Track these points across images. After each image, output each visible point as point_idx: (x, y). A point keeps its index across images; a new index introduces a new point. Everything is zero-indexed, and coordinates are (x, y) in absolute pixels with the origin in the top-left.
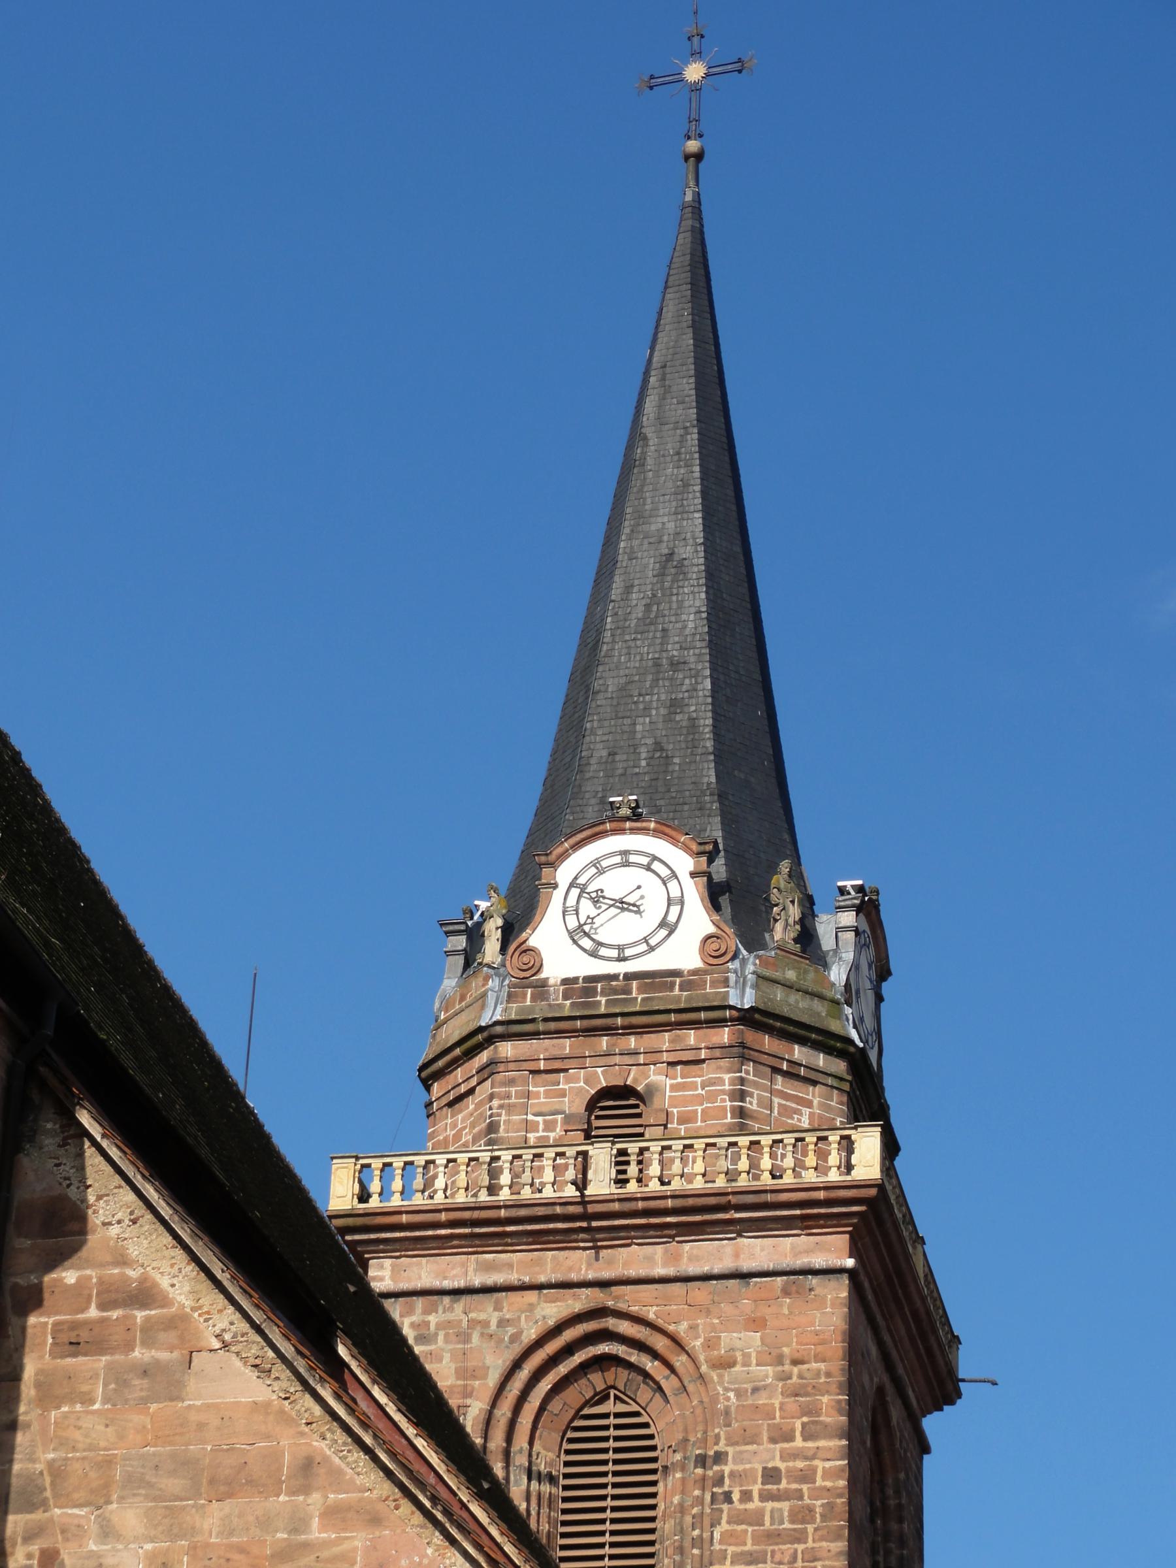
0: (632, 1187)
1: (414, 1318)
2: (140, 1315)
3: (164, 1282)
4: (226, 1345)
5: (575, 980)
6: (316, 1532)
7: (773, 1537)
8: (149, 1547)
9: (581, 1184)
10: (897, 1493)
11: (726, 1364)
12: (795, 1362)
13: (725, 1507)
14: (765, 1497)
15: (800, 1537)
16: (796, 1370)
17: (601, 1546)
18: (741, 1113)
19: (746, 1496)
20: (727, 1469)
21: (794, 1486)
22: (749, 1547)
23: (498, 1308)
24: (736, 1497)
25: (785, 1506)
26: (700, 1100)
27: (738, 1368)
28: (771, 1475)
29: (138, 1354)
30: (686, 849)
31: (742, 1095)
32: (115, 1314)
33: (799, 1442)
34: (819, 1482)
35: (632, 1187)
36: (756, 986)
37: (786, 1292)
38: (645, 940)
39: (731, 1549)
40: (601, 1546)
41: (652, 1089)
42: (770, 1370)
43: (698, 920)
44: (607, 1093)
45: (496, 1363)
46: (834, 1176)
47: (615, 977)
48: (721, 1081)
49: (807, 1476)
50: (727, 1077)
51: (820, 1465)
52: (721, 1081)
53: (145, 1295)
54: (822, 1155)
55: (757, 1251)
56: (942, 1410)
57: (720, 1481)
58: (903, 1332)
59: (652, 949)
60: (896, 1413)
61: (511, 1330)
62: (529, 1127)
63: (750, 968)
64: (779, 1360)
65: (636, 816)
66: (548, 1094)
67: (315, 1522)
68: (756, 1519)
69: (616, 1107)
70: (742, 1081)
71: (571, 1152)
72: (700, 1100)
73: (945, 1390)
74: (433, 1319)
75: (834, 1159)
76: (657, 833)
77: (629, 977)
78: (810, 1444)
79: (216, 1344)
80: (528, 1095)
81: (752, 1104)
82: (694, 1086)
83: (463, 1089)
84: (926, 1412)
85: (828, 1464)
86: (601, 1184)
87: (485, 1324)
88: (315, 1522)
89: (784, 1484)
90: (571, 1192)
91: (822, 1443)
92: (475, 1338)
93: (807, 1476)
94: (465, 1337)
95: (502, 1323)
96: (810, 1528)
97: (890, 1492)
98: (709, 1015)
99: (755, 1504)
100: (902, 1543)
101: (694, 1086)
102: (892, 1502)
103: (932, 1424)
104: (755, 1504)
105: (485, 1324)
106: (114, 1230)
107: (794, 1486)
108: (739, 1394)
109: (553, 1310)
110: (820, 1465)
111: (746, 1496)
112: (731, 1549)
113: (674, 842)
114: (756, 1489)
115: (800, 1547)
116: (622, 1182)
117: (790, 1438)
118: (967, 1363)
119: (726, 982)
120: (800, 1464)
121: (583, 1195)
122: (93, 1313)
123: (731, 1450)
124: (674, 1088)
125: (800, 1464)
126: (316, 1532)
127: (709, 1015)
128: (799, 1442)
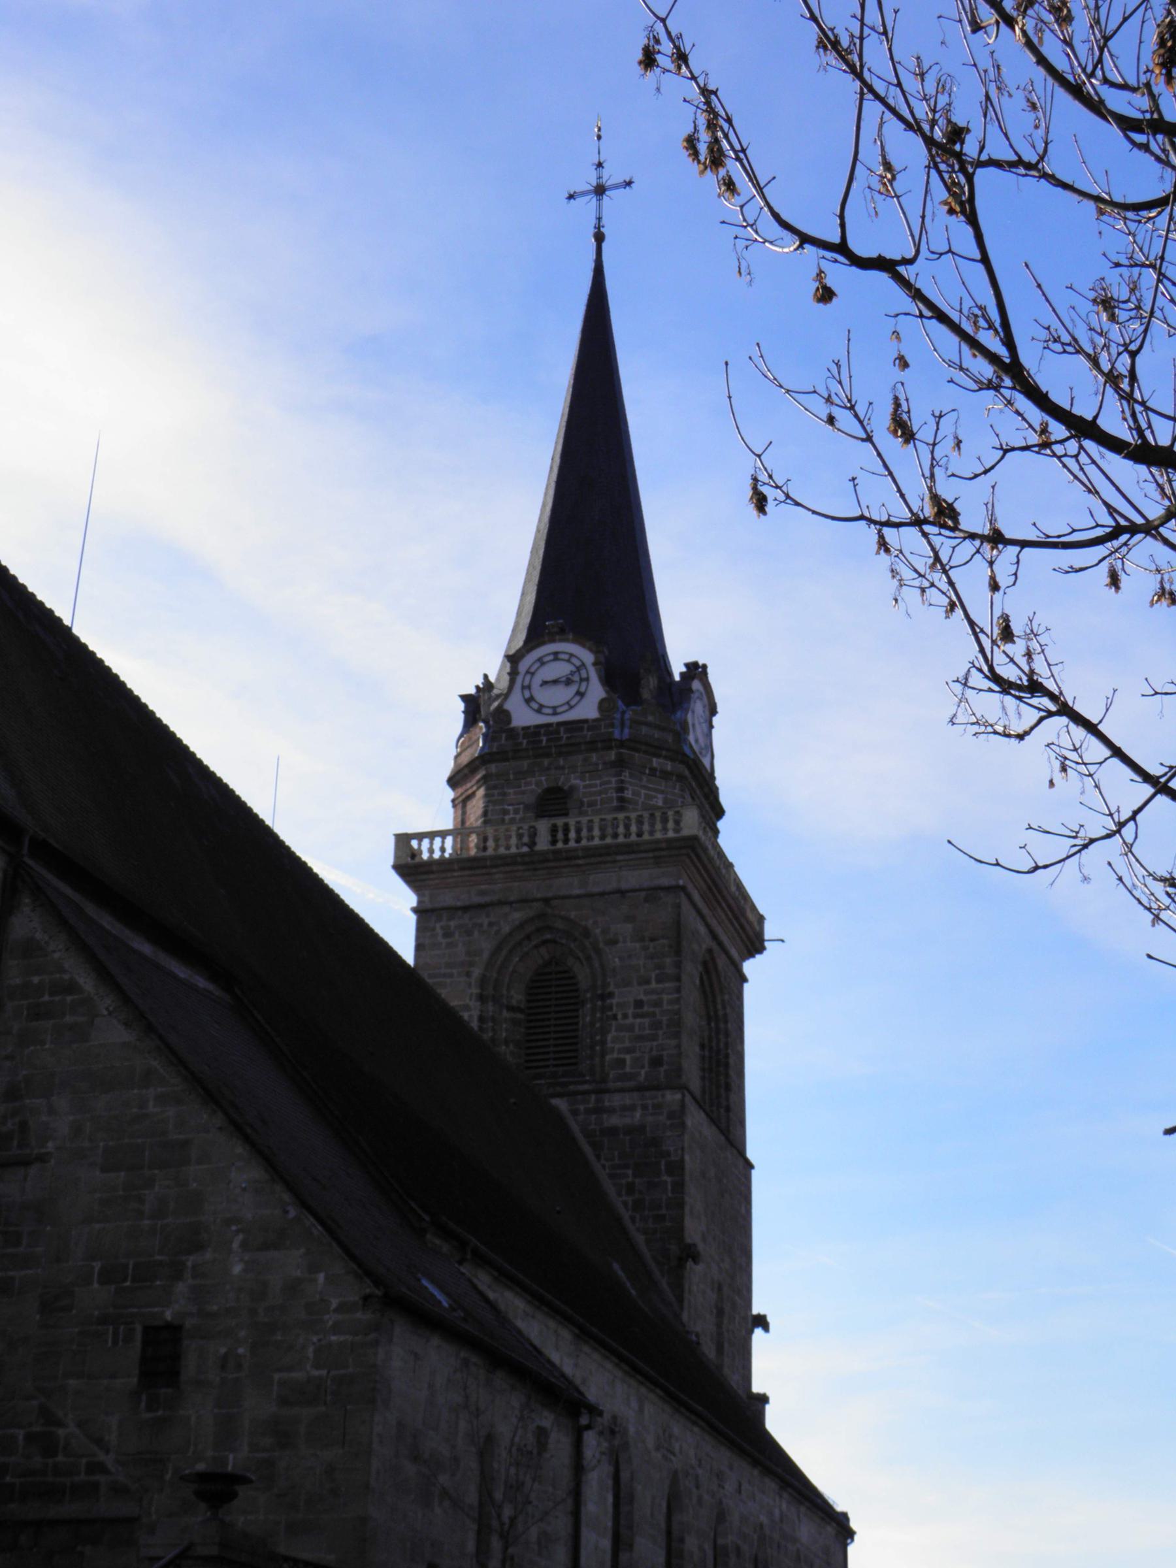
0: (560, 845)
1: (442, 923)
2: (69, 998)
3: (81, 981)
4: (110, 1013)
5: (528, 728)
6: (152, 1108)
7: (640, 1038)
8: (71, 1118)
9: (532, 844)
10: (724, 1008)
11: (614, 942)
12: (652, 940)
13: (614, 1023)
14: (636, 1016)
15: (654, 1038)
16: (652, 945)
17: (548, 1046)
18: (622, 800)
19: (625, 1016)
20: (614, 1001)
21: (652, 1009)
22: (627, 1044)
23: (488, 916)
24: (619, 1016)
25: (646, 1021)
26: (600, 793)
27: (620, 945)
28: (639, 1004)
29: (69, 1019)
30: (591, 650)
31: (621, 790)
32: (57, 998)
33: (654, 985)
34: (665, 1007)
35: (560, 845)
36: (631, 727)
37: (646, 900)
38: (568, 703)
39: (617, 1046)
40: (548, 1046)
41: (573, 789)
42: (638, 945)
43: (596, 691)
44: (548, 791)
45: (486, 946)
46: (671, 834)
47: (550, 725)
48: (609, 782)
49: (658, 1004)
50: (613, 780)
51: (665, 997)
52: (609, 782)
53: (71, 987)
54: (652, 825)
55: (634, 878)
56: (763, 1399)
57: (611, 1008)
58: (724, 917)
59: (571, 707)
60: (722, 961)
61: (495, 928)
62: (506, 812)
63: (627, 716)
64: (642, 939)
65: (562, 631)
66: (515, 793)
67: (151, 1103)
68: (630, 1028)
69: (553, 802)
70: (622, 781)
71: (526, 827)
72: (600, 793)
73: (755, 945)
74: (452, 924)
75: (671, 825)
76: (575, 641)
77: (559, 724)
78: (661, 986)
79: (105, 1013)
80: (504, 794)
81: (628, 794)
82: (596, 786)
83: (470, 792)
84: (745, 959)
85: (670, 997)
86: (543, 844)
87: (481, 925)
88: (151, 1103)
89: (646, 1009)
90: (525, 849)
91: (667, 985)
92: (476, 933)
93: (658, 1004)
94: (469, 933)
95: (491, 924)
96: (660, 1033)
97: (719, 1007)
98: (608, 743)
99: (630, 1020)
100: (727, 1035)
101: (596, 786)
102: (721, 1013)
103: (750, 967)
104: (630, 1020)
105: (481, 925)
106: (57, 955)
107: (652, 1009)
108: (621, 959)
109: (517, 916)
110: (665, 997)
111: (625, 1016)
112: (617, 1046)
113: (584, 646)
114: (630, 1011)
115: (655, 1043)
116: (554, 842)
117: (648, 982)
118: (769, 931)
119: (612, 725)
120: (654, 997)
121: (532, 850)
122: (46, 998)
123: (616, 991)
124: (585, 787)
125: (654, 997)
126: (152, 1108)
127: (608, 743)
128: (654, 985)
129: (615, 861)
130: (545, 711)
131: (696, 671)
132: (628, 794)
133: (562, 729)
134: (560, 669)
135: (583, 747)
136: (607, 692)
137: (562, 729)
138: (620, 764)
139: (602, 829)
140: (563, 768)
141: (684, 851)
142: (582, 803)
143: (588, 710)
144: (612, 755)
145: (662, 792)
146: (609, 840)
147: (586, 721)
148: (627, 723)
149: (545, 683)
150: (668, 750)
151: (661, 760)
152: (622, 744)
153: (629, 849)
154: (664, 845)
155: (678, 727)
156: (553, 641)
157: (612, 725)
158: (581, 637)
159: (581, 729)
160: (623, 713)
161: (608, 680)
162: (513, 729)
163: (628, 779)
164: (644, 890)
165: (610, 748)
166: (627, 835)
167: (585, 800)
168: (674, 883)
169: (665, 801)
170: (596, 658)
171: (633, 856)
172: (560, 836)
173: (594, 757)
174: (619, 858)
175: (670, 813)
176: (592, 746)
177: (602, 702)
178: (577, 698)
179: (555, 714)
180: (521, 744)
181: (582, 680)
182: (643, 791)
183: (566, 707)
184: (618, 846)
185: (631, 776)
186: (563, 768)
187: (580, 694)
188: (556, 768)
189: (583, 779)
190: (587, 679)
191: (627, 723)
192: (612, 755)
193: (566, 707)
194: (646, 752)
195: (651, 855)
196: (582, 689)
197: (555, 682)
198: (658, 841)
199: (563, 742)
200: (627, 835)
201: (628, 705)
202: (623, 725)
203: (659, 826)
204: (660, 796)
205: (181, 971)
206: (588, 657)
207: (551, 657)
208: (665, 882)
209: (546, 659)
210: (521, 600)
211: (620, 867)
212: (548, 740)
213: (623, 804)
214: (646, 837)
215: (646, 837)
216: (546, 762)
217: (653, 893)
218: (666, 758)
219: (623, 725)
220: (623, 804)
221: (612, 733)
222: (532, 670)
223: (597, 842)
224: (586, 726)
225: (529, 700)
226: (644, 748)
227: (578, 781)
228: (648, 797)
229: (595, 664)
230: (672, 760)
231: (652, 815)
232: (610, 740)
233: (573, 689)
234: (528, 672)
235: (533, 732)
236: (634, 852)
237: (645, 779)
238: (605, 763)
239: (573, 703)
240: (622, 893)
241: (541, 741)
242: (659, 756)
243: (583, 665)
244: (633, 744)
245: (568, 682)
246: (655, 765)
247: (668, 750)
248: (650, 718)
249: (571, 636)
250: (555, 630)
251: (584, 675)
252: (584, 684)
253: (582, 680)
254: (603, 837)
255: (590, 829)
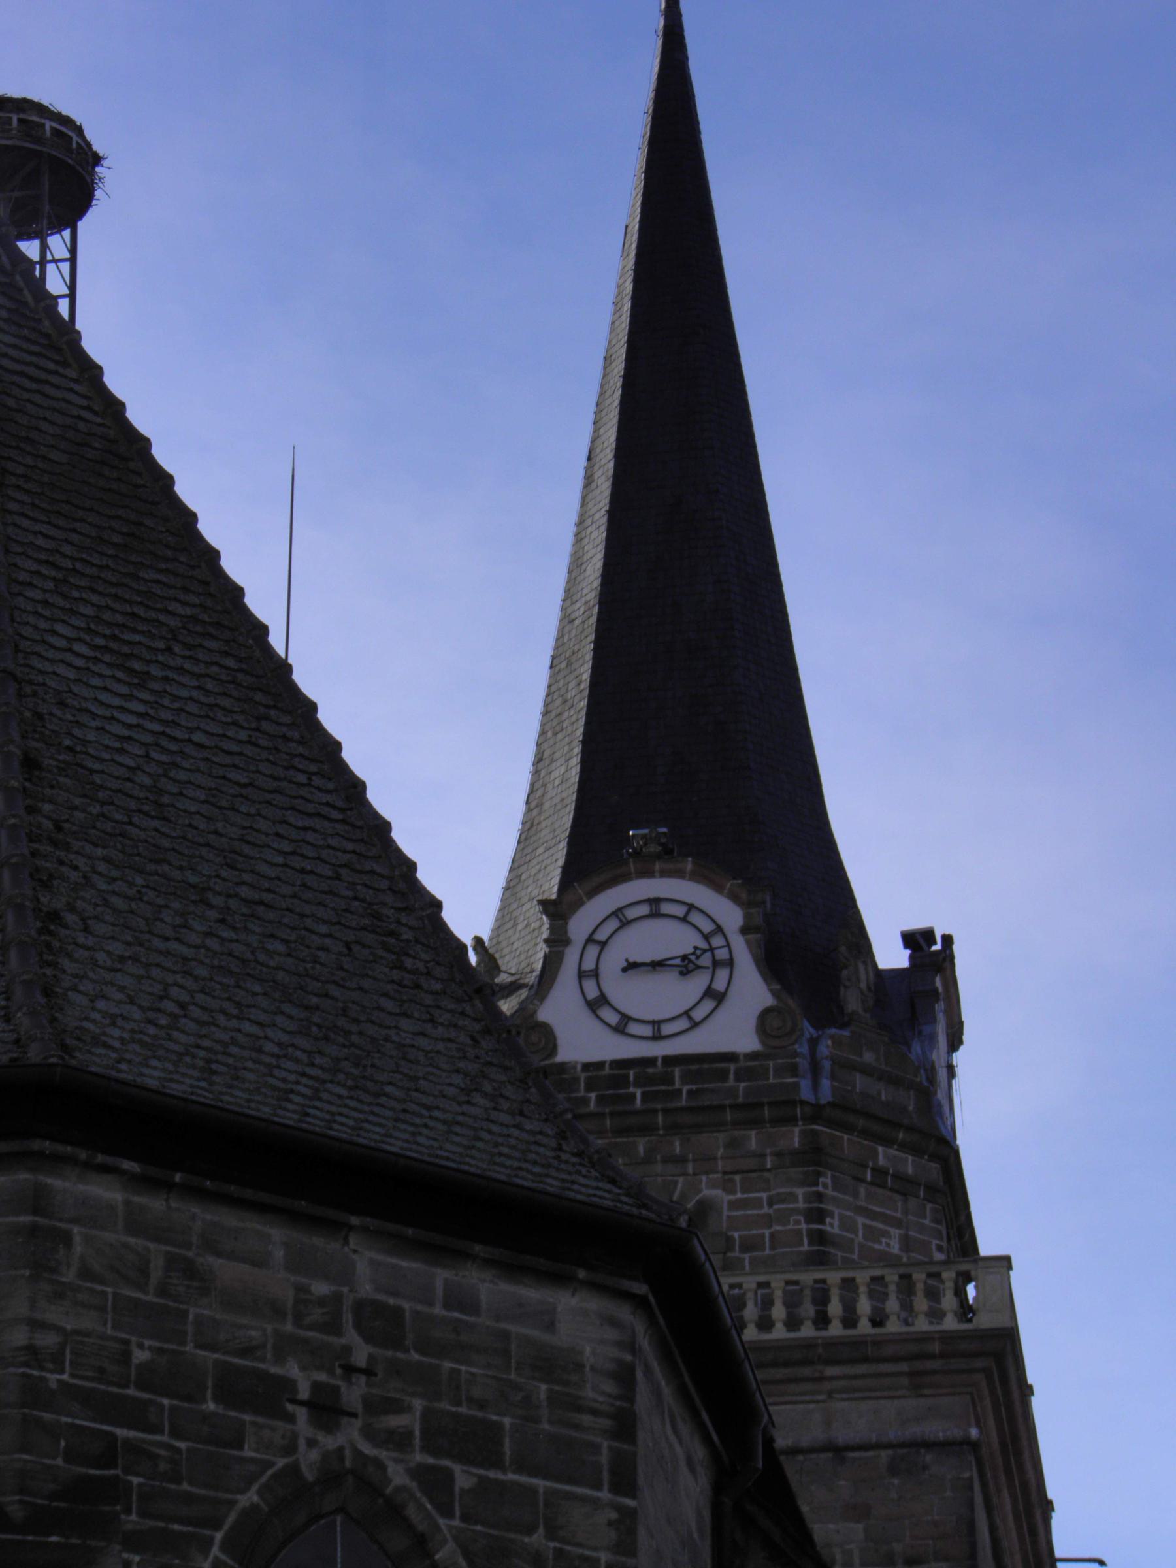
5: (600, 1065)
26: (768, 1220)
30: (734, 898)
31: (817, 1215)
36: (833, 1077)
37: (893, 1469)
41: (705, 1209)
43: (751, 992)
47: (650, 1061)
48: (793, 1197)
50: (800, 1192)
59: (695, 1025)
70: (820, 1197)
72: (768, 1220)
77: (670, 1061)
81: (832, 1226)
82: (758, 1203)
98: (785, 1109)
101: (758, 1203)
113: (718, 888)
119: (794, 1070)
124: (733, 1205)
127: (785, 1109)
129: (821, 1379)
130: (634, 1028)
131: (930, 953)
132: (832, 1226)
133: (677, 1072)
134: (673, 939)
135: (729, 1116)
136: (774, 993)
137: (677, 1072)
138: (813, 1156)
139: (792, 1304)
140: (682, 1160)
141: (979, 1363)
142: (729, 1240)
143: (734, 1030)
144: (794, 1137)
145: (898, 1224)
146: (807, 1331)
147: (731, 1057)
148: (827, 1065)
149: (631, 966)
150: (910, 1129)
151: (893, 1152)
152: (816, 1113)
153: (855, 1352)
154: (936, 1347)
155: (922, 1077)
156: (647, 873)
157: (794, 1070)
158: (711, 871)
159: (723, 1075)
160: (814, 1043)
161: (773, 962)
162: (563, 1067)
163: (830, 1192)
164: (889, 1446)
165: (791, 1120)
166: (850, 1320)
167: (736, 1235)
168: (957, 1433)
169: (907, 1244)
170: (747, 917)
171: (862, 1369)
172: (808, 1309)
173: (753, 1140)
174: (831, 1371)
175: (919, 1276)
176: (749, 1113)
177: (764, 1016)
178: (708, 1005)
179: (657, 1037)
180: (585, 1101)
181: (716, 964)
182: (861, 1221)
183: (683, 1024)
184: (831, 1344)
185: (837, 1186)
186: (682, 1160)
187: (716, 996)
188: (665, 1161)
189: (728, 1188)
190: (730, 963)
191: (827, 1065)
192: (794, 1137)
193: (683, 1024)
194: (865, 1133)
195: (904, 1367)
196: (720, 985)
197: (657, 965)
198: (925, 1338)
199: (683, 1102)
200: (850, 1320)
201: (818, 1025)
202: (815, 1070)
203: (921, 1303)
204: (896, 1232)
205: (282, 1555)
206: (730, 915)
207: (644, 910)
208: (937, 1429)
209: (631, 914)
210: (536, 773)
211: (830, 1394)
212: (600, 1100)
213: (821, 1251)
214: (893, 1326)
215: (893, 1326)
216: (641, 1145)
217: (909, 1455)
218: (903, 1147)
219: (815, 1070)
220: (821, 1251)
221: (796, 1086)
222: (601, 936)
223: (779, 1332)
224: (732, 1067)
225: (597, 1004)
226: (861, 1122)
227: (718, 1192)
228: (872, 1234)
229: (744, 930)
230: (917, 1151)
231: (906, 1277)
232: (792, 1103)
233: (696, 985)
234: (590, 940)
235: (612, 1077)
236: (866, 1360)
237: (862, 1190)
238: (778, 1155)
239: (698, 1015)
240: (838, 1451)
241: (633, 1096)
242: (888, 1142)
243: (719, 929)
244: (841, 1113)
245: (686, 966)
246: (881, 1161)
247: (910, 1129)
248: (868, 1057)
249: (689, 865)
250: (653, 848)
251: (722, 954)
252: (722, 974)
253: (716, 964)
254: (793, 1323)
255: (768, 1303)
